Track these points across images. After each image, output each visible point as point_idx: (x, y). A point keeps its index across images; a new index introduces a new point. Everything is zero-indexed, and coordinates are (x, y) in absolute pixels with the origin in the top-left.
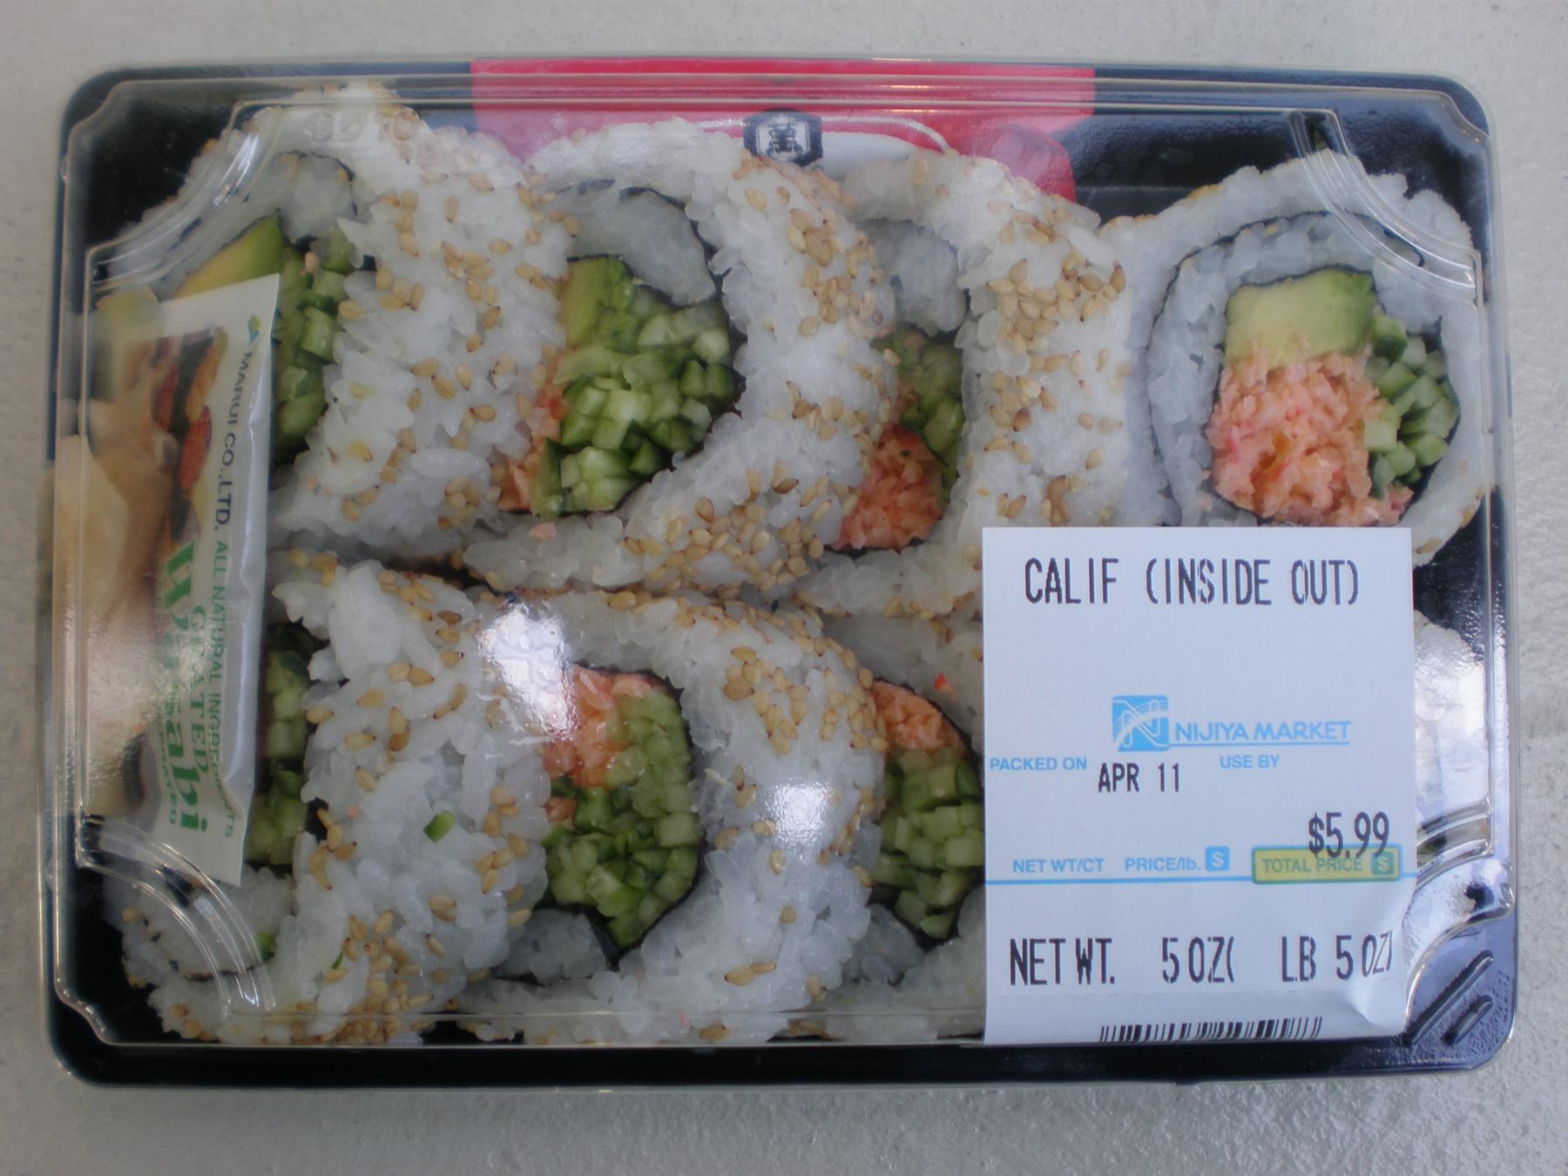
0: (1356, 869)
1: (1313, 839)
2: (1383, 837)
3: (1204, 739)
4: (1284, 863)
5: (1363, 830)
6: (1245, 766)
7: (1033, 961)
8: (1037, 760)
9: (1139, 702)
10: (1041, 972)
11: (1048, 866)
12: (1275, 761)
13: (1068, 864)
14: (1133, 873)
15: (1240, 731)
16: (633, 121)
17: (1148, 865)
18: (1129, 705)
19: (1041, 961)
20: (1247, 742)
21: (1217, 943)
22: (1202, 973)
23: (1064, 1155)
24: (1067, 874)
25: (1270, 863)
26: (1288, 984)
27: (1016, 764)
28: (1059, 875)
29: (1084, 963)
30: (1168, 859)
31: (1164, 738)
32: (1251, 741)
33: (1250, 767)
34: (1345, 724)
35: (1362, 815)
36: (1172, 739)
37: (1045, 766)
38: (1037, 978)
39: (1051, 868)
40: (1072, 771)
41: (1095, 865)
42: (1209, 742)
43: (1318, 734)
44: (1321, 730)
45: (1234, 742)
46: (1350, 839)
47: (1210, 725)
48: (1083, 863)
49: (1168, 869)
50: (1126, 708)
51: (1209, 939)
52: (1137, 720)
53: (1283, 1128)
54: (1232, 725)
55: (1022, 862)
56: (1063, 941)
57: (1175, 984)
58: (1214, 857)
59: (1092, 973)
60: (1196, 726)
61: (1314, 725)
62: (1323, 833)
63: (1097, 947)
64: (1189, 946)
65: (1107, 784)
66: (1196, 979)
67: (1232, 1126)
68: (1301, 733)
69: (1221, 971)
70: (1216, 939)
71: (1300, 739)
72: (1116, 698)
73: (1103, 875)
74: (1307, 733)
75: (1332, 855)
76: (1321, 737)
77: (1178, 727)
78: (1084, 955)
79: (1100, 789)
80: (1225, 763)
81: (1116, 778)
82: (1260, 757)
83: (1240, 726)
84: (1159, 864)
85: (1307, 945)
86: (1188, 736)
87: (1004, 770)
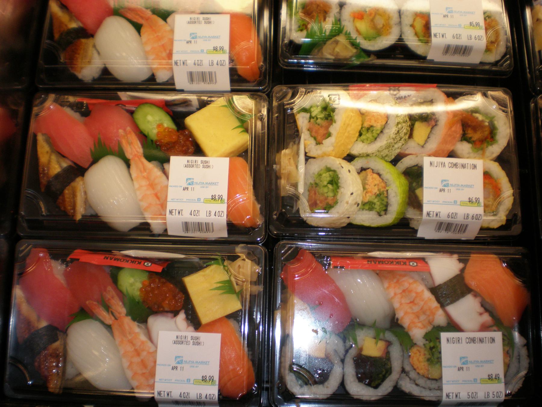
10: (173, 214)
14: (187, 201)
29: (179, 213)
31: (182, 362)
36: (449, 185)
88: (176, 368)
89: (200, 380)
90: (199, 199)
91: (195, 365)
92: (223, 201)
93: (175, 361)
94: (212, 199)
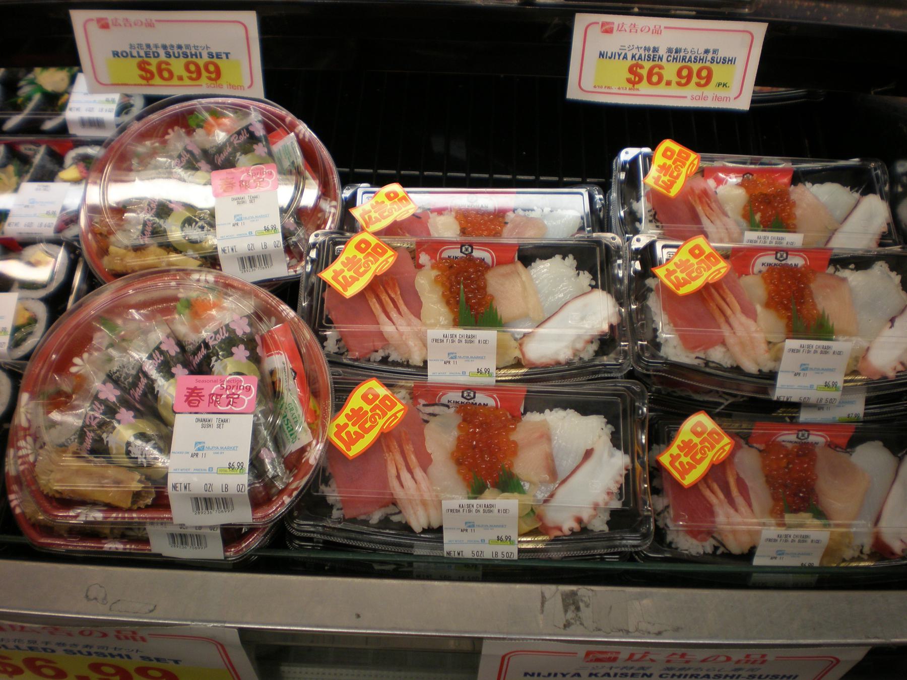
16: (21, 397)
31: (204, 448)
48: (186, 470)
57: (679, 679)
90: (211, 469)
91: (220, 451)
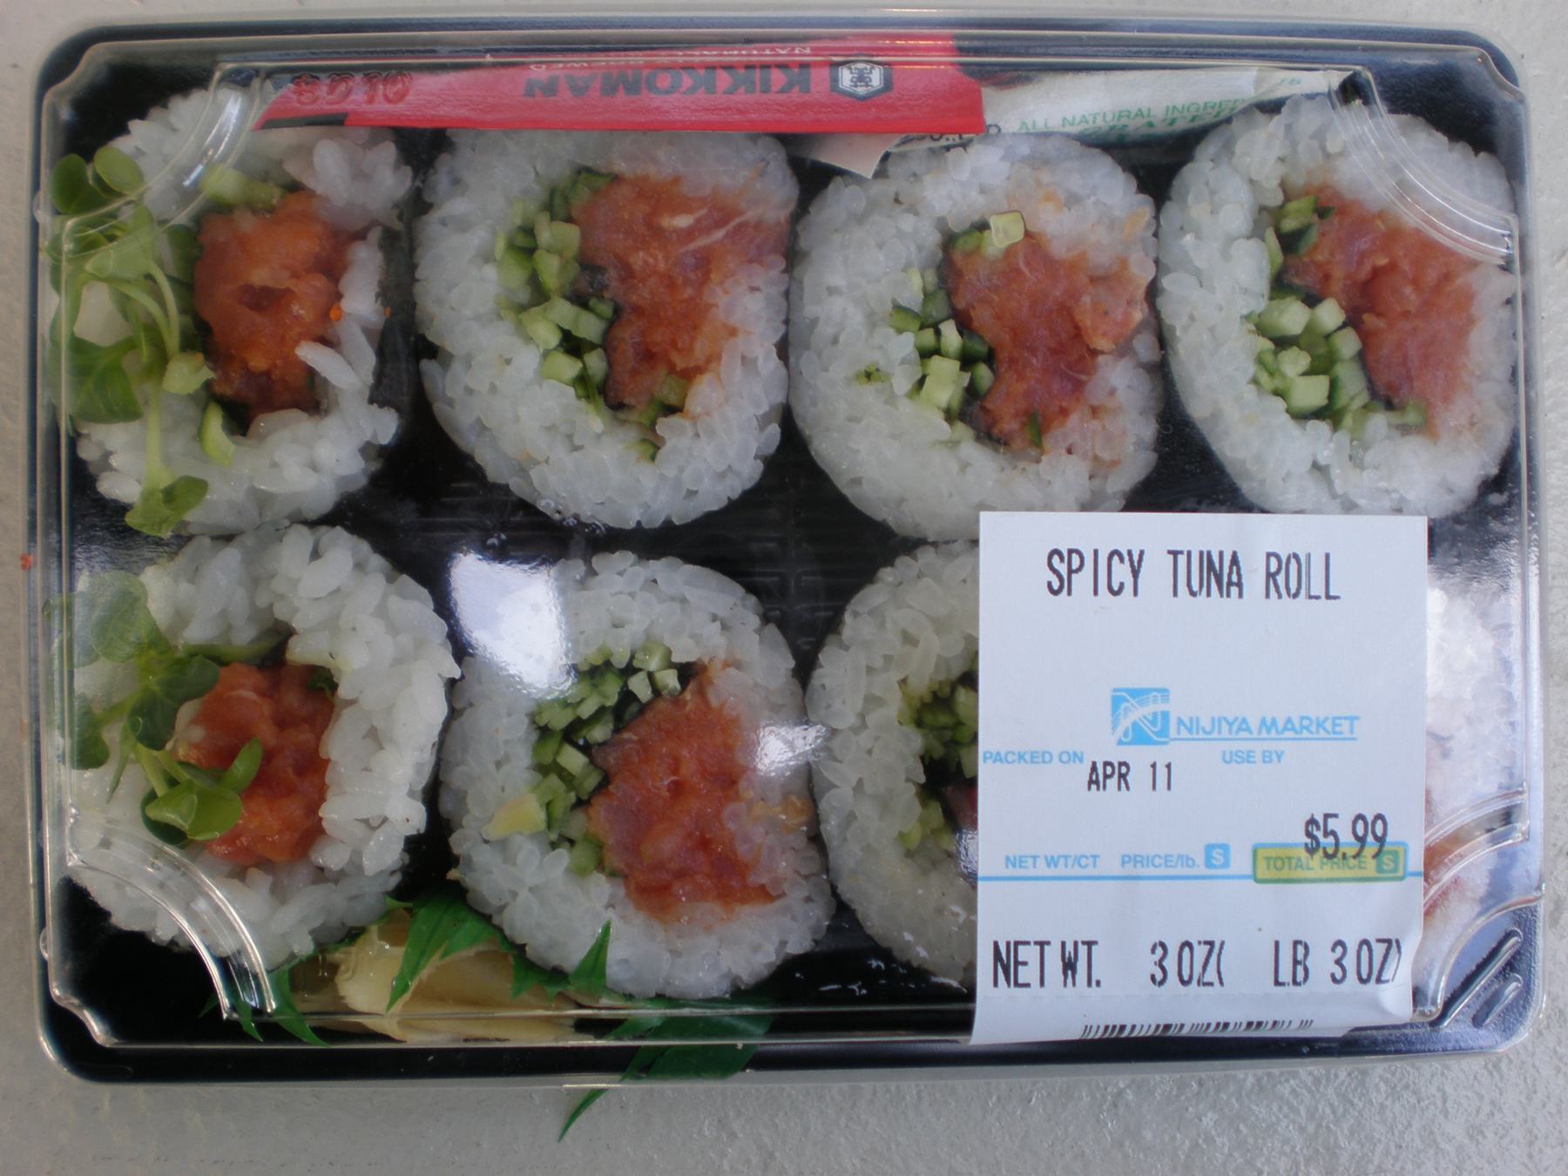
0: (1360, 868)
1: (1309, 841)
2: (1381, 840)
3: (1206, 733)
4: (1286, 861)
5: (1360, 832)
6: (1248, 762)
7: (1017, 963)
8: (1032, 753)
9: (1139, 694)
10: (1025, 974)
11: (1041, 863)
12: (1279, 757)
13: (1062, 860)
15: (1244, 725)
17: (1145, 862)
18: (1128, 697)
19: (1025, 964)
20: (1250, 736)
21: (1385, 945)
22: (1191, 977)
23: (1280, 1109)
24: (1061, 870)
25: (1272, 862)
26: (1279, 988)
27: (1010, 758)
28: (1052, 872)
29: (1069, 966)
30: (1166, 856)
31: (1164, 732)
32: (1255, 735)
33: (1254, 762)
34: (1352, 719)
35: (1360, 817)
36: (1173, 733)
37: (1040, 759)
38: (1021, 980)
39: (1044, 865)
40: (1067, 765)
41: (1091, 861)
42: (1212, 736)
43: (1324, 729)
44: (1328, 725)
45: (1238, 737)
46: (1346, 837)
47: (1213, 719)
48: (1078, 860)
49: (1166, 866)
50: (1127, 701)
51: (1200, 943)
52: (1137, 713)
53: (1491, 1074)
54: (1236, 719)
55: (1015, 858)
56: (1048, 943)
58: (1214, 855)
59: (1077, 976)
60: (1198, 719)
61: (1321, 719)
62: (1319, 834)
63: (1083, 950)
64: (1178, 949)
65: (1097, 782)
66: (1184, 983)
67: (1443, 1074)
68: (1307, 728)
69: (1210, 975)
70: (1206, 943)
71: (1305, 734)
72: (1115, 690)
73: (1096, 872)
74: (1313, 728)
75: (1327, 855)
76: (1328, 732)
77: (1180, 721)
78: (1070, 958)
79: (1089, 788)
80: (1228, 758)
81: (1106, 777)
82: (1264, 752)
83: (1244, 720)
84: (1157, 861)
85: (1301, 950)
86: (1190, 730)
87: (998, 763)
88: (1121, 772)
89: (1296, 845)
92: (1395, 853)
93: (1115, 723)
94: (1311, 851)
